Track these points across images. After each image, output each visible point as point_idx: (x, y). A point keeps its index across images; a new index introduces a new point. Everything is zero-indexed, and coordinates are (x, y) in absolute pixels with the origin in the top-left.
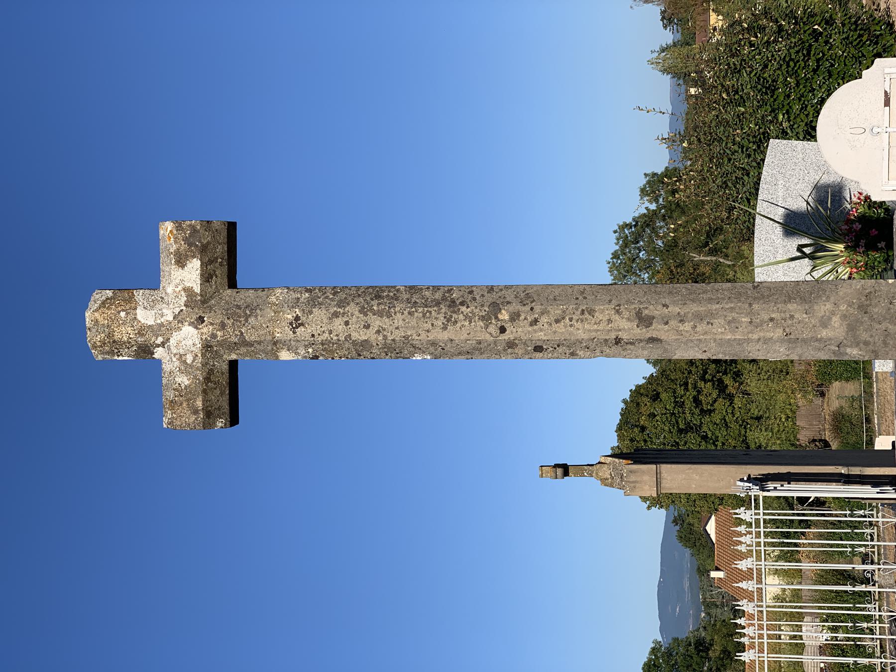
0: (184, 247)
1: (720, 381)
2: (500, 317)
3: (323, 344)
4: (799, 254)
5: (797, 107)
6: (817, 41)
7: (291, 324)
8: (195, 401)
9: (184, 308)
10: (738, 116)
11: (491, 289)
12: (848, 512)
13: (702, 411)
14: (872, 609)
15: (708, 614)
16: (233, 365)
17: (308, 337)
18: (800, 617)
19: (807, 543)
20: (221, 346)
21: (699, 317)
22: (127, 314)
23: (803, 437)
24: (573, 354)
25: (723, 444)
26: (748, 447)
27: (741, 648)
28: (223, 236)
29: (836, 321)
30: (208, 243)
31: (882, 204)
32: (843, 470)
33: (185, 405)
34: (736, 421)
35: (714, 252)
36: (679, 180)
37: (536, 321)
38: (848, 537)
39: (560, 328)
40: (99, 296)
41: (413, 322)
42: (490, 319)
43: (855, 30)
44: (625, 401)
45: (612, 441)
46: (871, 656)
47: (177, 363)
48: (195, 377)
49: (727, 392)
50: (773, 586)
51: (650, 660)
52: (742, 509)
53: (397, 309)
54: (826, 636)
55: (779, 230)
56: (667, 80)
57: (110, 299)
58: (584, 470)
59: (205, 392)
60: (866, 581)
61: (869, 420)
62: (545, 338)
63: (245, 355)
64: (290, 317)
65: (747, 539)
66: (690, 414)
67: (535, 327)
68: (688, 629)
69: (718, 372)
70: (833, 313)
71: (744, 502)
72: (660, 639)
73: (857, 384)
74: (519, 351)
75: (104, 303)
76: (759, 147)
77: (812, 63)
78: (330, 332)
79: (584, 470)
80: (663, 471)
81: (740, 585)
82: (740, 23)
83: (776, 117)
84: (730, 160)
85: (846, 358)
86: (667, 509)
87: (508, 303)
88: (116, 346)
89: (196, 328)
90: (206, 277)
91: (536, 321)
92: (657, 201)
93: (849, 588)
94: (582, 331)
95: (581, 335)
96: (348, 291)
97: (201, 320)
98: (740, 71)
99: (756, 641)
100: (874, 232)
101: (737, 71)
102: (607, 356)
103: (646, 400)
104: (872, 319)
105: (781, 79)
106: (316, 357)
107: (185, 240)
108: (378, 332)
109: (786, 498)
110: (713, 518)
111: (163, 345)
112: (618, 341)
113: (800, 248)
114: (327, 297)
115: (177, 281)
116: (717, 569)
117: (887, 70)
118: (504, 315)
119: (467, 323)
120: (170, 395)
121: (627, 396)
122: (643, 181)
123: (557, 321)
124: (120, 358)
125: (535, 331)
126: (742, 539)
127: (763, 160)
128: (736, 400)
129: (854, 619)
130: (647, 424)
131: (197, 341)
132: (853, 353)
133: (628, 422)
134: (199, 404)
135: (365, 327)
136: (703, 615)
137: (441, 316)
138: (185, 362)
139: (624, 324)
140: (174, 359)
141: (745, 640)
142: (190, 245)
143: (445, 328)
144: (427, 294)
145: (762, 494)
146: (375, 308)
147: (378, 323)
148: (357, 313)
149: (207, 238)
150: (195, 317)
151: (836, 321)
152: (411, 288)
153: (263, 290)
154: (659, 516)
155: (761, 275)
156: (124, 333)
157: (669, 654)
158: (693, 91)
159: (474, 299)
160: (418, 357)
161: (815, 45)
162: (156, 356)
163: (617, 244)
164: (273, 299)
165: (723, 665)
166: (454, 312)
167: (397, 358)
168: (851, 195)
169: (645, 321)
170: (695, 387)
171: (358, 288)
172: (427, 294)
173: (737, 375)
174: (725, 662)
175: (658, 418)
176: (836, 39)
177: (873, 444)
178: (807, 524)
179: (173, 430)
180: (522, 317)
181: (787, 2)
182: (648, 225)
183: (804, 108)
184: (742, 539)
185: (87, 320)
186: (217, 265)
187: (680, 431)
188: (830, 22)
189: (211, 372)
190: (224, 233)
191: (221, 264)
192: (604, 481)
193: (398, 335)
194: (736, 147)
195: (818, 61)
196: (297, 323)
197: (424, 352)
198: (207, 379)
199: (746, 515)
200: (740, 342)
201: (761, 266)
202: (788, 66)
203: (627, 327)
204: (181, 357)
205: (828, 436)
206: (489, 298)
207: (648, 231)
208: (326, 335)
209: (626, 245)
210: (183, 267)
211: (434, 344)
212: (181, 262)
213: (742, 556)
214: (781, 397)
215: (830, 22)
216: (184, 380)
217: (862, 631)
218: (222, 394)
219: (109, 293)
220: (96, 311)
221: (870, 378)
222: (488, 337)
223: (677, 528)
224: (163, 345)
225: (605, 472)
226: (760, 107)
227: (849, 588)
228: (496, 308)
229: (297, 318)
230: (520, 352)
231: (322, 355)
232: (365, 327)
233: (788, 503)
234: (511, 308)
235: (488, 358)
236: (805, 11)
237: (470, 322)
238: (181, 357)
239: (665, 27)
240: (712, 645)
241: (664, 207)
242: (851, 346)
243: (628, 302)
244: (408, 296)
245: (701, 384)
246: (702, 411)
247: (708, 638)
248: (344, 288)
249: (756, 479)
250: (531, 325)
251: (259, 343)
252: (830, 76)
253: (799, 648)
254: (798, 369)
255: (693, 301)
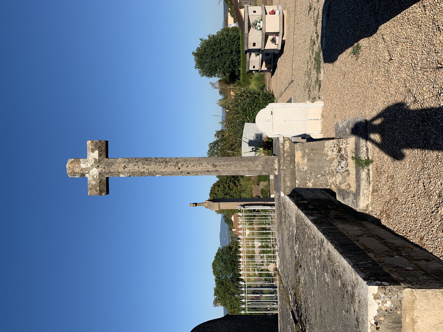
0: (94, 147)
1: (235, 182)
2: (179, 165)
3: (132, 173)
4: (252, 150)
5: (251, 115)
6: (256, 99)
7: (123, 167)
8: (97, 188)
9: (94, 163)
10: (238, 117)
11: (176, 158)
12: (264, 213)
13: (230, 189)
14: (270, 236)
15: (232, 240)
16: (107, 178)
17: (128, 171)
18: (254, 239)
19: (256, 221)
20: (104, 173)
21: (228, 165)
22: (78, 165)
23: (254, 195)
24: (197, 174)
25: (235, 197)
26: (241, 198)
27: (240, 247)
28: (104, 145)
29: (260, 166)
30: (100, 146)
31: (271, 138)
32: (263, 203)
33: (94, 189)
34: (238, 192)
35: (233, 150)
36: (224, 132)
37: (188, 166)
38: (264, 219)
39: (194, 168)
40: (70, 160)
41: (156, 167)
42: (176, 166)
43: (265, 96)
44: (211, 187)
45: (208, 197)
46: (271, 248)
47: (92, 178)
48: (97, 182)
49: (236, 185)
50: (248, 232)
51: (218, 252)
52: (239, 213)
53: (152, 163)
54: (260, 244)
55: (247, 145)
56: (221, 108)
57: (73, 161)
58: (201, 204)
59: (99, 185)
60: (269, 230)
61: (269, 191)
62: (190, 170)
63: (111, 175)
64: (123, 165)
65: (240, 220)
66: (227, 190)
67: (187, 168)
68: (227, 244)
69: (234, 180)
70: (259, 164)
71: (240, 211)
72: (220, 247)
73: (266, 182)
74: (184, 174)
75: (71, 162)
76: (243, 124)
77: (255, 104)
78: (134, 169)
79: (201, 204)
80: (220, 204)
81: (239, 232)
82: (238, 94)
83: (246, 117)
84: (236, 128)
85: (262, 175)
86: (222, 214)
87: (181, 162)
88: (75, 174)
89: (97, 169)
90: (100, 155)
91: (188, 166)
92: (219, 138)
93: (265, 231)
94: (199, 169)
95: (199, 170)
96: (139, 159)
97: (98, 166)
98: (238, 106)
99: (243, 245)
100: (269, 145)
101: (237, 106)
102: (206, 175)
103: (216, 187)
104: (268, 165)
105: (248, 108)
106: (130, 176)
107: (94, 145)
108: (147, 169)
109: (250, 210)
110: (233, 216)
111: (88, 173)
112: (208, 171)
113: (252, 149)
114: (133, 160)
115: (92, 156)
116: (234, 228)
117: (272, 106)
118: (180, 165)
119: (170, 167)
120: (90, 186)
121: (212, 186)
122: (216, 133)
123: (193, 166)
124: (76, 177)
125: (188, 169)
126: (239, 220)
127: (244, 128)
128: (238, 187)
129: (266, 239)
130: (217, 193)
131: (97, 172)
132: (264, 174)
133: (212, 193)
134: (98, 189)
135: (143, 168)
136: (231, 240)
137: (163, 165)
138: (94, 178)
139: (210, 167)
140: (91, 177)
141: (240, 245)
142: (95, 147)
143: (164, 168)
144: (160, 159)
145: (244, 209)
146: (146, 163)
147: (147, 167)
148: (141, 164)
149: (100, 145)
150: (97, 166)
151: (260, 166)
152: (156, 158)
153: (116, 159)
154: (220, 216)
155: (243, 155)
156: (77, 170)
157: (222, 250)
158: (227, 111)
159: (172, 161)
160: (157, 176)
161: (256, 100)
162: (86, 176)
163: (209, 148)
164: (118, 161)
165: (236, 253)
166: (167, 164)
167: (152, 176)
168: (264, 136)
169: (215, 166)
170: (229, 184)
171: (141, 158)
172: (160, 159)
173: (239, 180)
174: (236, 252)
175: (220, 191)
176: (260, 99)
177: (270, 197)
178: (255, 216)
179: (91, 196)
180: (184, 165)
181: (438, 1)
182: (217, 144)
183: (253, 115)
184: (239, 220)
185: (67, 167)
186: (103, 152)
187: (225, 194)
188: (259, 94)
189: (101, 180)
190: (105, 144)
191: (104, 152)
192: (206, 207)
193: (152, 170)
194: (237, 124)
195: (256, 104)
196: (125, 167)
197: (159, 174)
198: (100, 182)
199: (240, 214)
200: (238, 171)
201: (244, 153)
202: (249, 105)
203: (211, 168)
204: (93, 177)
205: (260, 195)
206: (176, 161)
207: (217, 145)
208: (133, 170)
209: (211, 148)
210: (93, 152)
211: (161, 172)
212: (93, 151)
213: (240, 224)
214: (249, 185)
215: (259, 94)
216: (94, 183)
217: (268, 242)
218: (104, 186)
219: (73, 160)
220: (69, 164)
221: (270, 181)
222: (175, 170)
223: (224, 219)
224: (88, 173)
225: (206, 205)
226: (243, 115)
227: (265, 231)
228: (177, 163)
229: (125, 166)
230: (184, 174)
231: (132, 175)
232: (143, 168)
233: (250, 211)
234: (181, 163)
235: (176, 176)
236: (253, 91)
237: (171, 167)
238: (93, 177)
239: (220, 95)
240: (233, 248)
241: (220, 139)
242: (263, 172)
243: (211, 161)
244: (155, 160)
245: (230, 183)
246: (230, 189)
247: (232, 246)
248: (137, 158)
249: (243, 205)
250: (186, 167)
251: (115, 172)
252: (259, 108)
253: (254, 247)
254: (253, 179)
255: (226, 161)
